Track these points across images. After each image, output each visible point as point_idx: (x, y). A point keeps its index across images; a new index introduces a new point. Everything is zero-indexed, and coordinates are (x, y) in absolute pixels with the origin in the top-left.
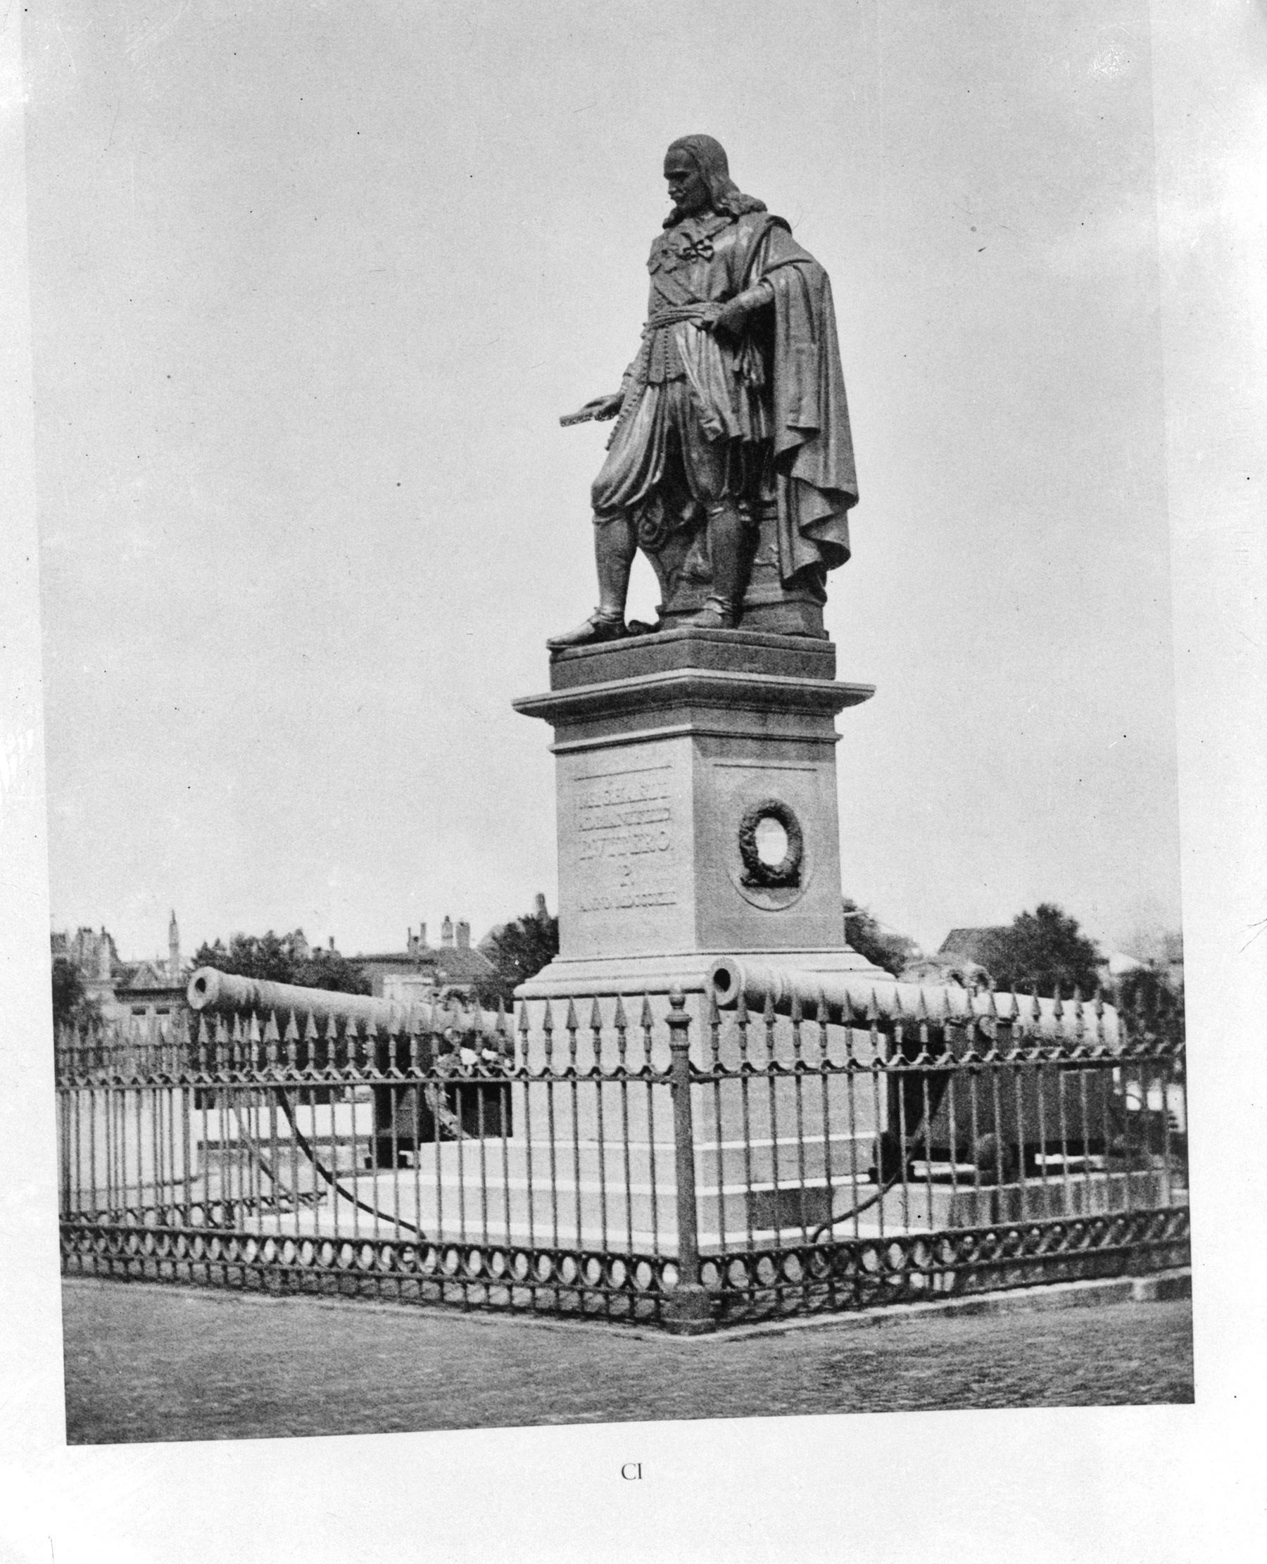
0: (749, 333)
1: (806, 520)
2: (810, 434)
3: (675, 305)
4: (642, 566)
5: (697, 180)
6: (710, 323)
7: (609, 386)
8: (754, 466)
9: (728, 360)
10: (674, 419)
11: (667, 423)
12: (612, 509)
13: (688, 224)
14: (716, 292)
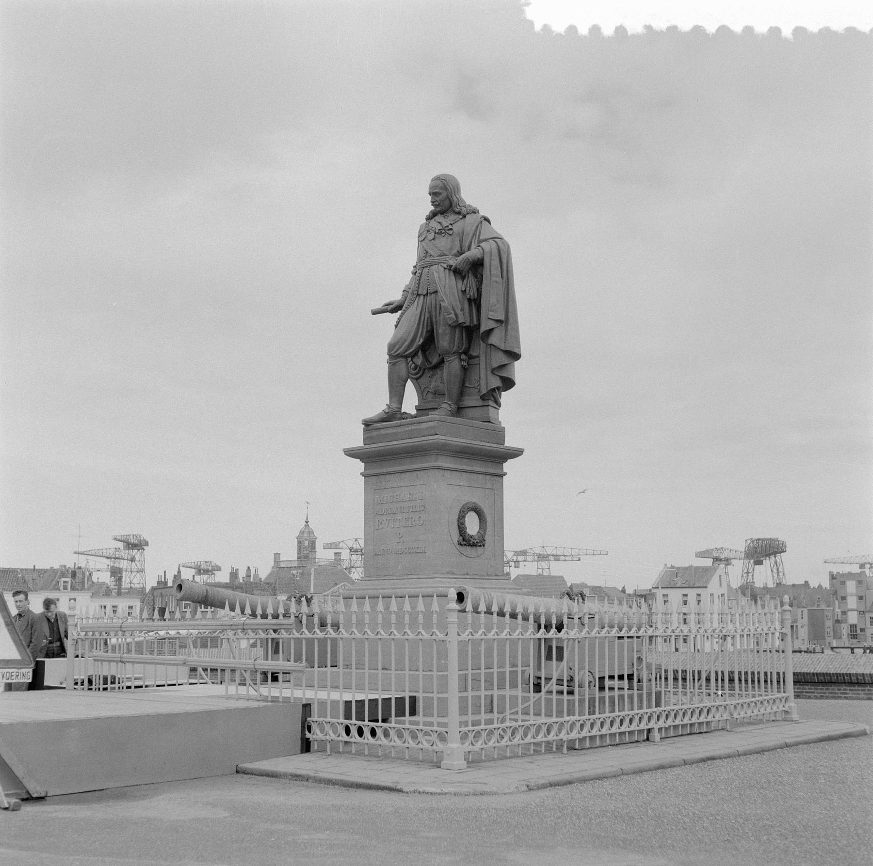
1: (495, 365)
4: (410, 387)
5: (445, 201)
6: (451, 266)
7: (396, 296)
8: (471, 333)
9: (460, 282)
10: (430, 312)
11: (427, 315)
12: (398, 356)
13: (439, 218)
14: (455, 252)
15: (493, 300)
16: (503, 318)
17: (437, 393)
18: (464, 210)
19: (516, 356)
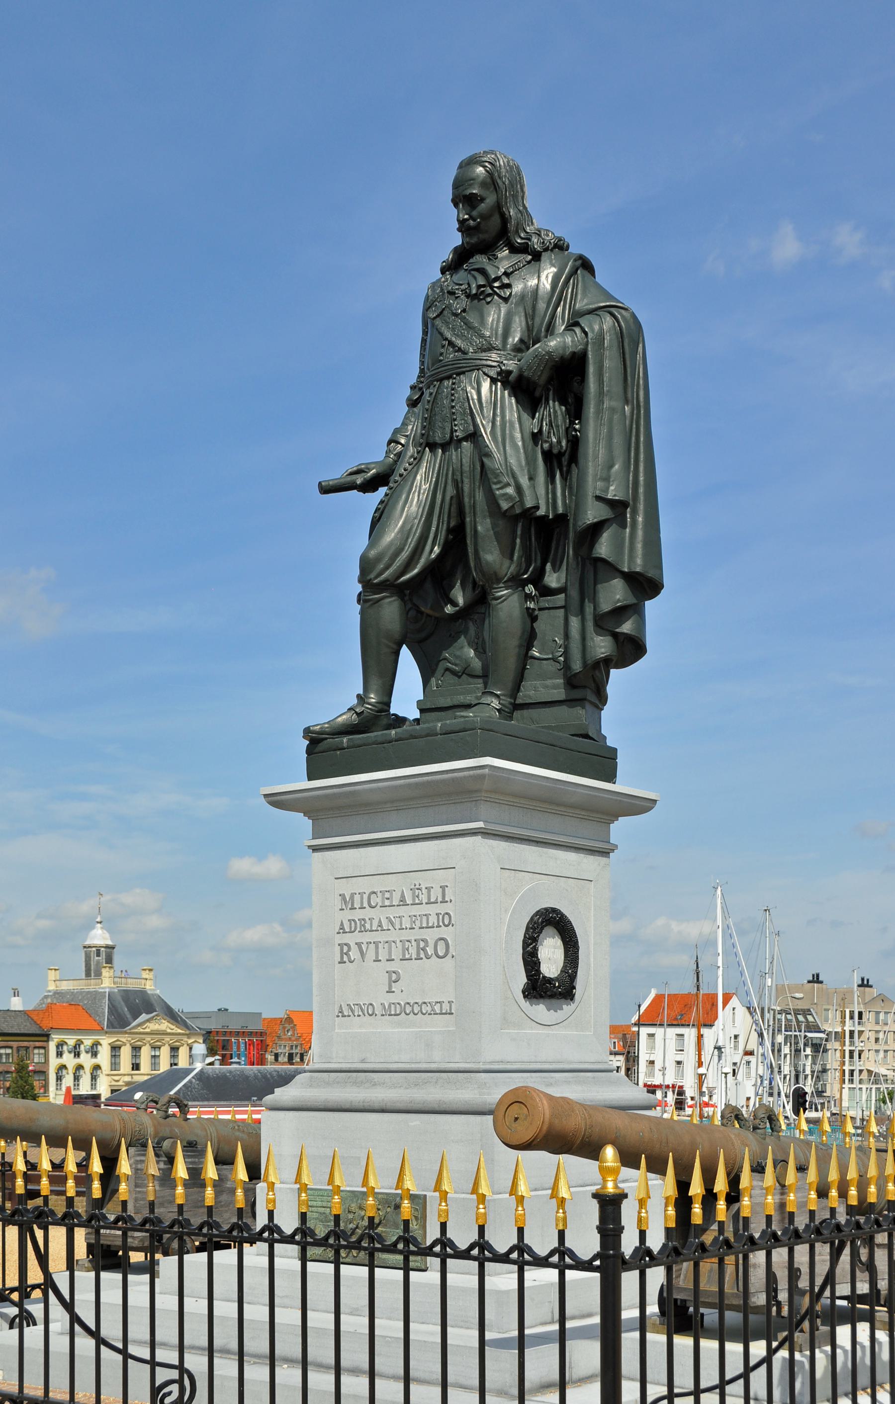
0: (550, 385)
1: (606, 606)
2: (619, 507)
3: (465, 353)
6: (509, 372)
7: (374, 454)
9: (525, 416)
10: (458, 485)
11: (451, 491)
12: (385, 586)
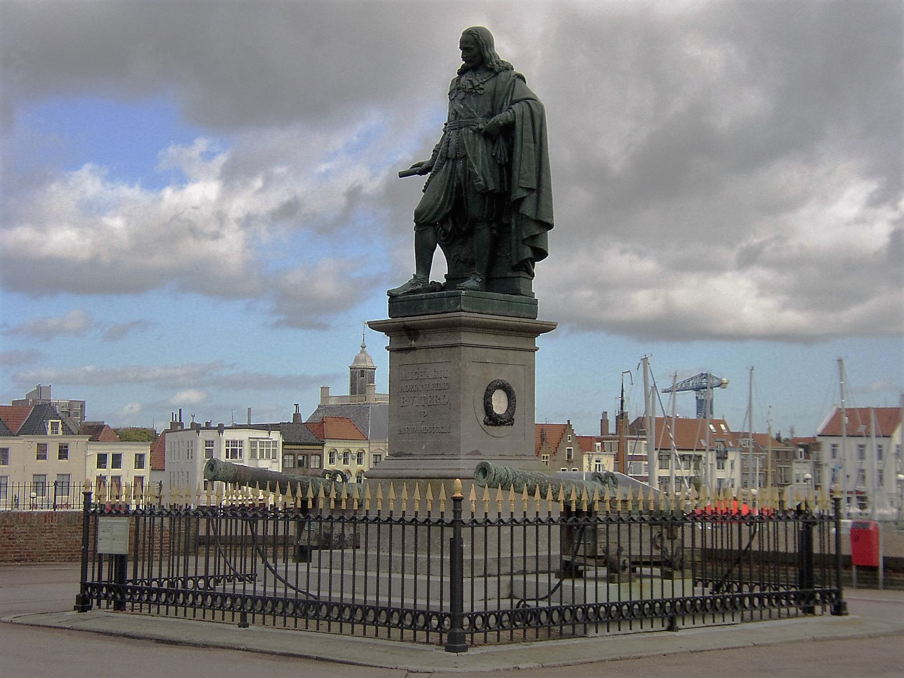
4: (439, 254)
15: (525, 167)
16: (533, 185)
17: (470, 263)
18: (497, 69)
19: (550, 226)
